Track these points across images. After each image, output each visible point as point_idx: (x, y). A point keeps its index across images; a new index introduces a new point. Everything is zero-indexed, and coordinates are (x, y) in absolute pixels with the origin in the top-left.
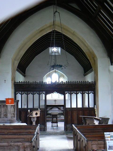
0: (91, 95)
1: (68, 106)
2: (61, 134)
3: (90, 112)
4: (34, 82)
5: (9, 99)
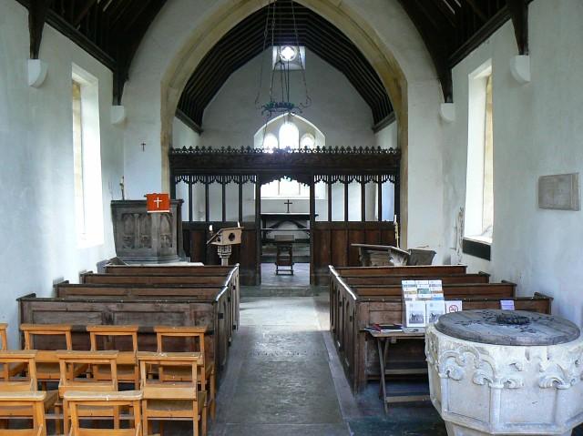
0: (388, 187)
1: (322, 217)
2: (301, 293)
3: (381, 234)
4: (226, 148)
5: (155, 196)
